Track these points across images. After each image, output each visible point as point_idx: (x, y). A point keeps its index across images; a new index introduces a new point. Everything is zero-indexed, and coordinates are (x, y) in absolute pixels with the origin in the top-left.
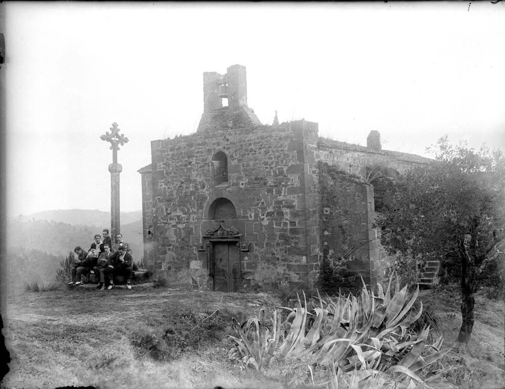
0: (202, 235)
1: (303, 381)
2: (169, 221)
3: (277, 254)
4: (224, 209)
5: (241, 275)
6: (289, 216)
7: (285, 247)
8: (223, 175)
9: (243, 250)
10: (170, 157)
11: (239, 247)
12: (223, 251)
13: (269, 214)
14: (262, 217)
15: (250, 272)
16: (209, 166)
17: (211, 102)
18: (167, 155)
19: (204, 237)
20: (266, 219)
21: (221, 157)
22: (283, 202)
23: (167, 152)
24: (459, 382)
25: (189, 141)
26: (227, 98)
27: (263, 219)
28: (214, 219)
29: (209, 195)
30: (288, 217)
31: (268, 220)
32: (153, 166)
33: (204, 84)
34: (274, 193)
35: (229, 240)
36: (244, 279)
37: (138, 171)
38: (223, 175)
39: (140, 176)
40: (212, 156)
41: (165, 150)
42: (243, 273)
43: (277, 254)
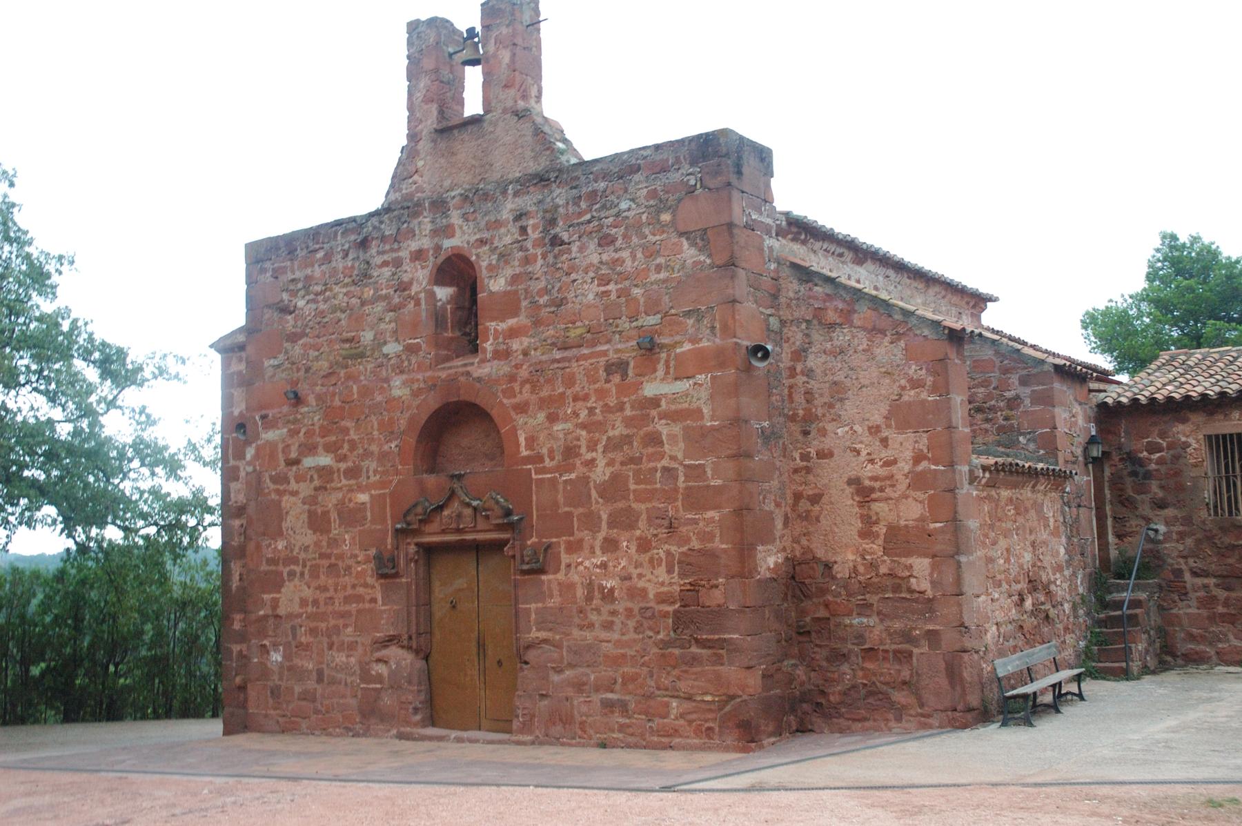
0: (394, 523)
1: (916, 651)
2: (293, 486)
3: (640, 576)
4: (468, 439)
5: (518, 650)
6: (682, 445)
7: (668, 553)
8: (465, 321)
9: (525, 567)
10: (300, 285)
11: (514, 557)
12: (453, 582)
13: (613, 445)
14: (589, 456)
15: (545, 641)
16: (418, 303)
17: (438, 123)
18: (293, 280)
19: (397, 530)
20: (601, 462)
21: (458, 271)
22: (663, 403)
23: (293, 272)
24: (649, 614)
25: (355, 233)
26: (752, 548)
27: (593, 460)
28: (431, 471)
29: (406, 392)
30: (675, 449)
31: (608, 465)
32: (252, 328)
33: (408, 57)
34: (630, 373)
35: (480, 537)
36: (526, 663)
37: (211, 346)
38: (465, 321)
39: (217, 358)
40: (427, 272)
41: (285, 267)
42: (522, 643)
43: (640, 576)
